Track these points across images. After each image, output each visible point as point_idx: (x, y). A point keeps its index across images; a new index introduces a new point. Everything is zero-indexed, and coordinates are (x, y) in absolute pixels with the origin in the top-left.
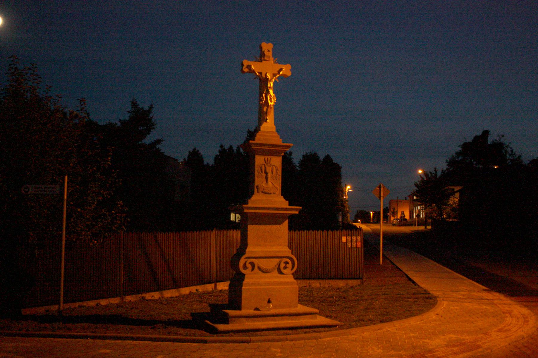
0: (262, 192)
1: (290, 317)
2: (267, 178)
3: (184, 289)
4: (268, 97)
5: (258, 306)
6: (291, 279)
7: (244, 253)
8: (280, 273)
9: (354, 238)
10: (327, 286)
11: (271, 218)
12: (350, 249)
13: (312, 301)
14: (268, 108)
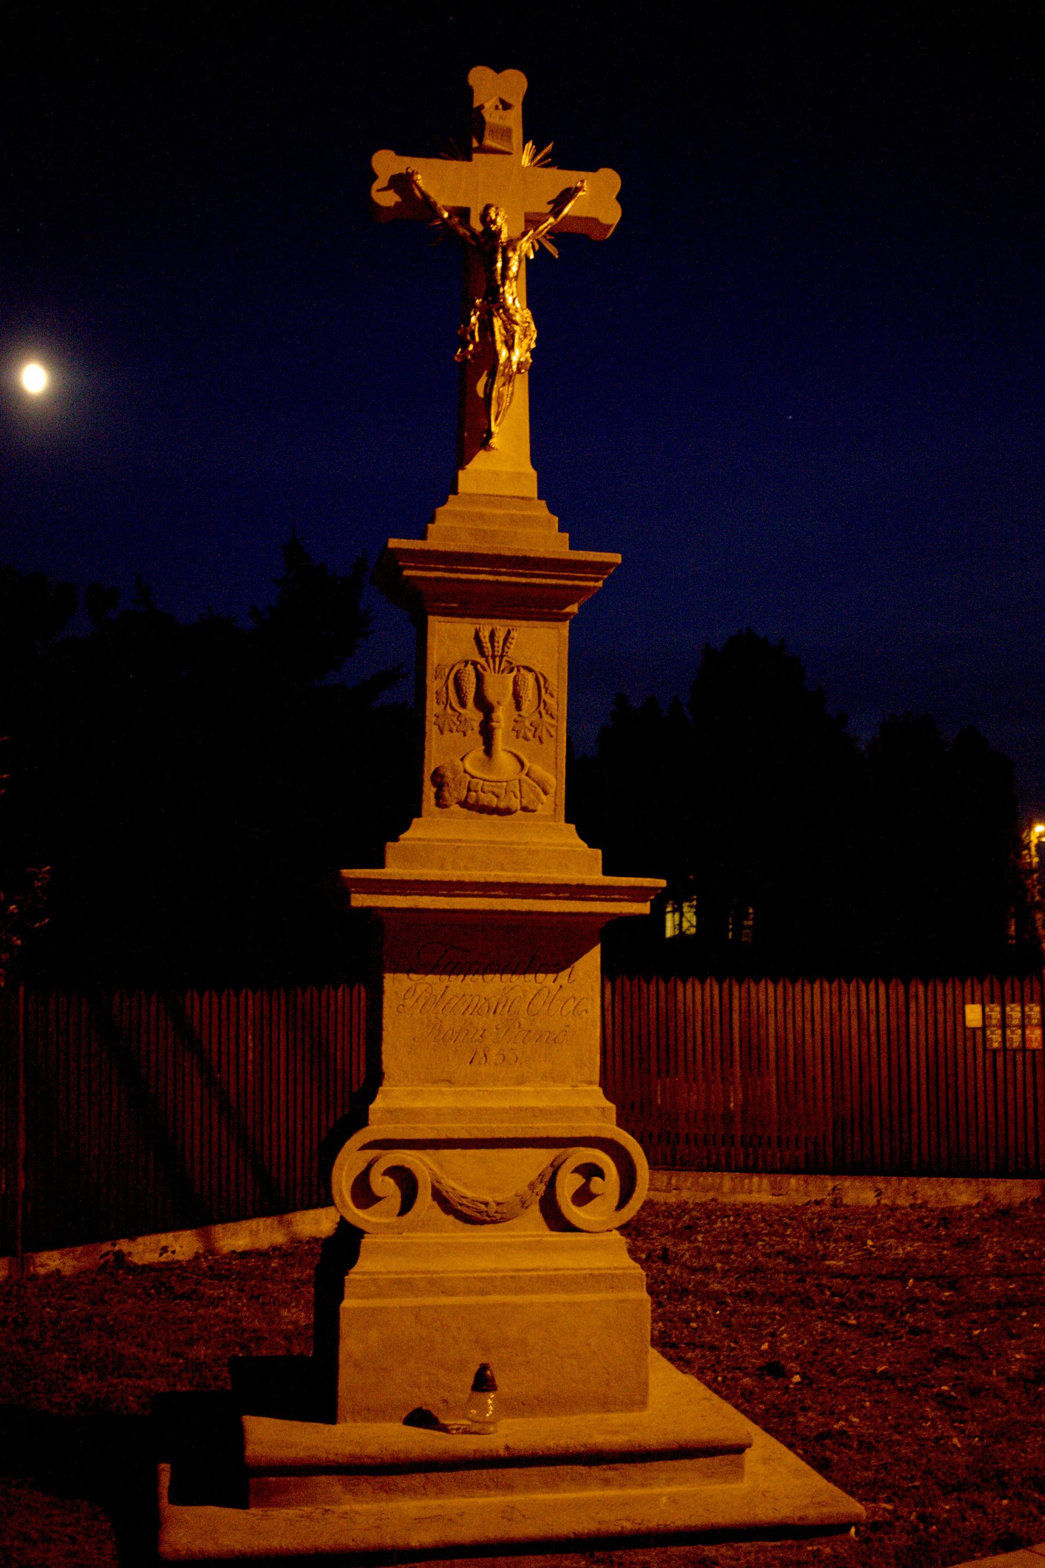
0: (464, 804)
1: (596, 1471)
2: (487, 732)
3: (311, 1214)
4: (497, 323)
5: (428, 1400)
6: (613, 1256)
7: (362, 1121)
8: (557, 1221)
9: (1015, 1012)
10: (903, 1201)
11: (513, 940)
12: (1000, 1059)
13: (806, 1302)
14: (492, 376)
